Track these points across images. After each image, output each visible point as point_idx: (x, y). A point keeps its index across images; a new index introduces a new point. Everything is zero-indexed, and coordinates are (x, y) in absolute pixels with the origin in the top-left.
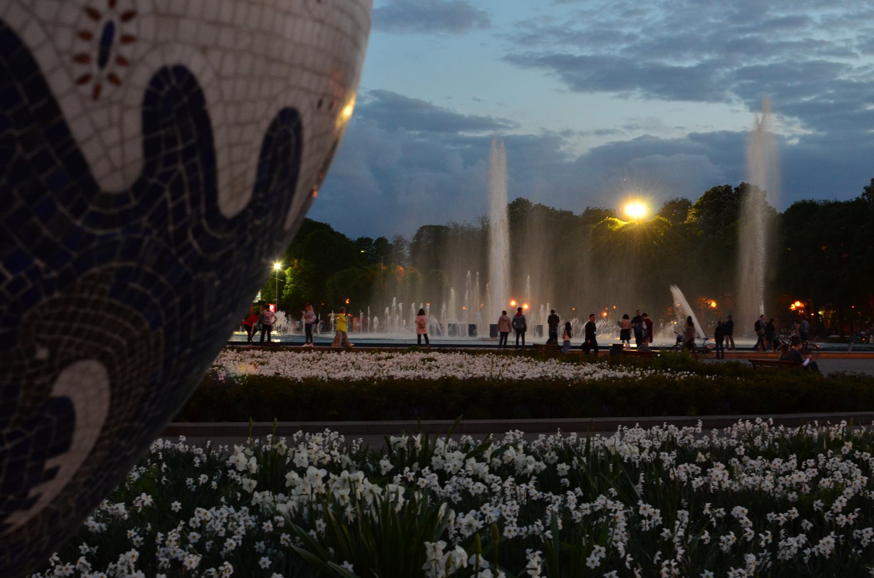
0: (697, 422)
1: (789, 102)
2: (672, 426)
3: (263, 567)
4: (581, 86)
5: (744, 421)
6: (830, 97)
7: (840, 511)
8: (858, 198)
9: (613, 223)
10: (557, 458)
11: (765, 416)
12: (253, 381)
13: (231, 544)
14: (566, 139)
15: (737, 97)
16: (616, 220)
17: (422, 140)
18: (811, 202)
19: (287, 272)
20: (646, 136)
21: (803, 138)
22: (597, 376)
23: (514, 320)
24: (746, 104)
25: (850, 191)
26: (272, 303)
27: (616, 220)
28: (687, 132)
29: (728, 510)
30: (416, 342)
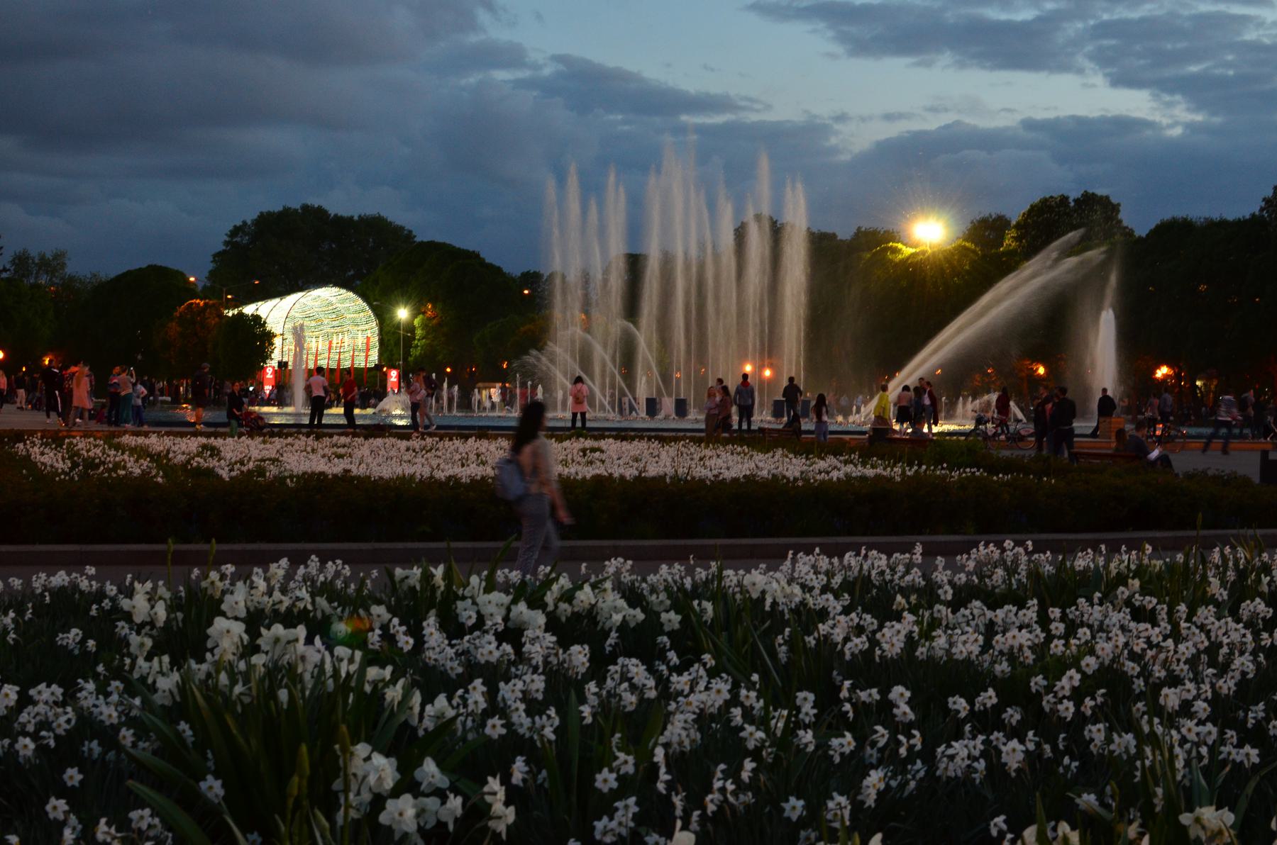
0: (913, 545)
1: (1169, 72)
2: (875, 552)
3: (69, 784)
4: (861, 48)
5: (986, 546)
6: (1229, 65)
7: (1068, 694)
8: (1253, 215)
9: (896, 251)
10: (668, 602)
11: (1018, 537)
12: (314, 481)
13: (26, 746)
14: (837, 127)
15: (1092, 65)
16: (900, 246)
17: (626, 128)
18: (1185, 220)
19: (417, 322)
20: (958, 123)
21: (1190, 126)
22: (835, 475)
23: (738, 391)
24: (1106, 75)
25: (1242, 204)
26: (394, 367)
27: (900, 246)
28: (1018, 117)
29: (885, 692)
30: (569, 425)
